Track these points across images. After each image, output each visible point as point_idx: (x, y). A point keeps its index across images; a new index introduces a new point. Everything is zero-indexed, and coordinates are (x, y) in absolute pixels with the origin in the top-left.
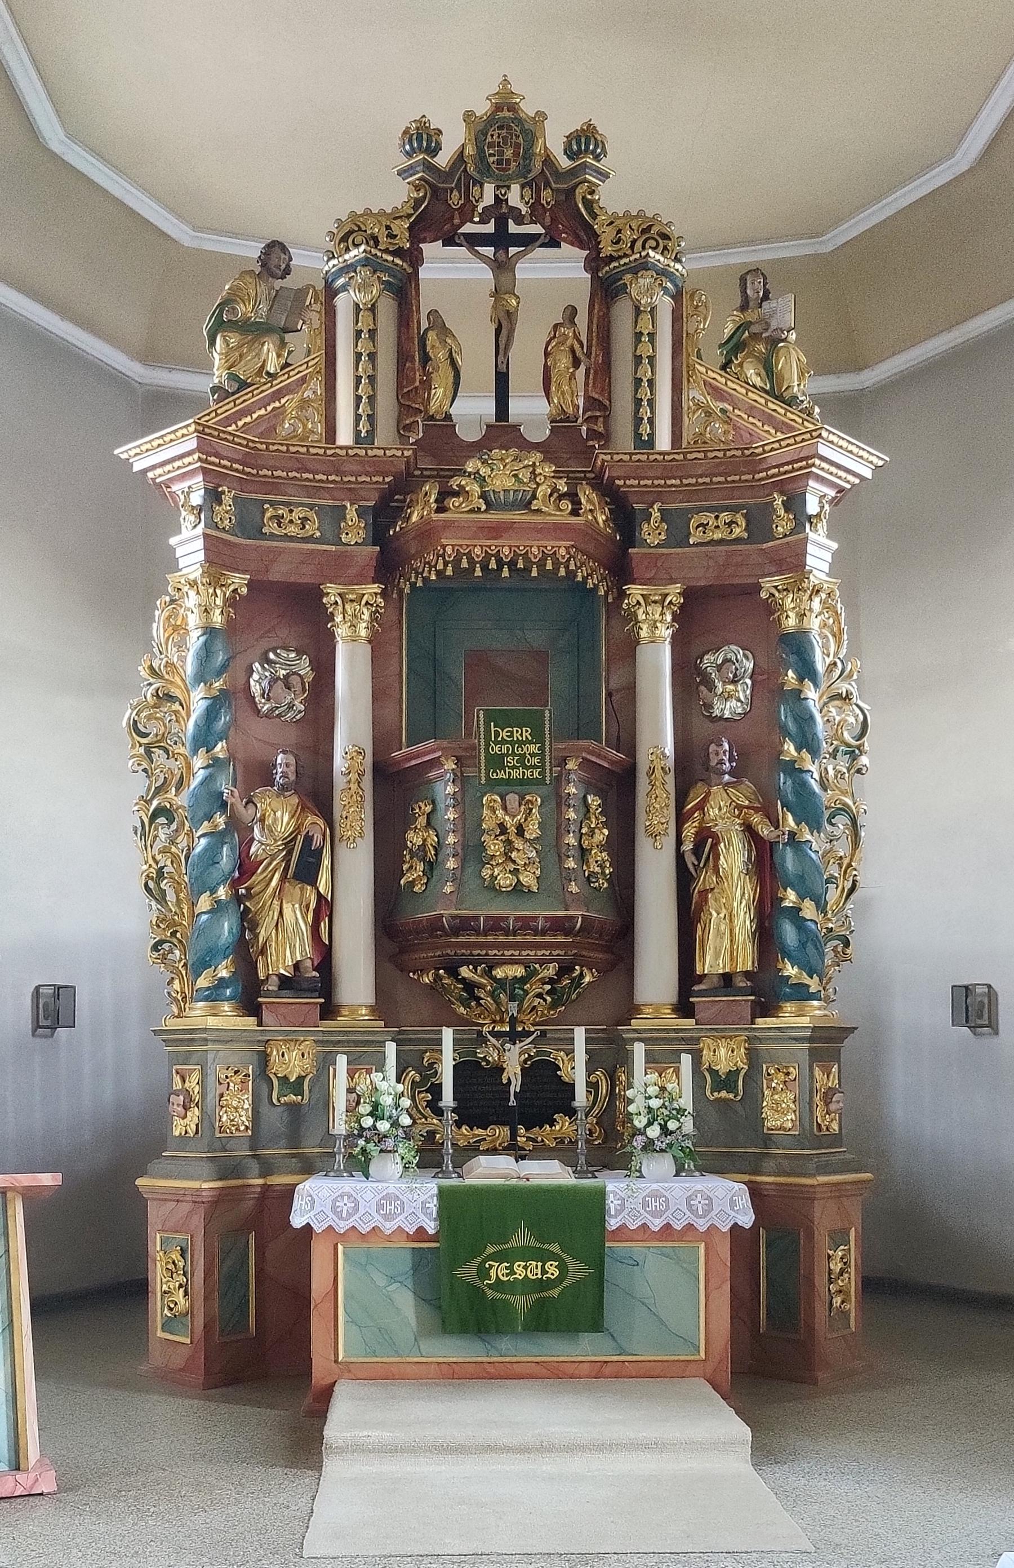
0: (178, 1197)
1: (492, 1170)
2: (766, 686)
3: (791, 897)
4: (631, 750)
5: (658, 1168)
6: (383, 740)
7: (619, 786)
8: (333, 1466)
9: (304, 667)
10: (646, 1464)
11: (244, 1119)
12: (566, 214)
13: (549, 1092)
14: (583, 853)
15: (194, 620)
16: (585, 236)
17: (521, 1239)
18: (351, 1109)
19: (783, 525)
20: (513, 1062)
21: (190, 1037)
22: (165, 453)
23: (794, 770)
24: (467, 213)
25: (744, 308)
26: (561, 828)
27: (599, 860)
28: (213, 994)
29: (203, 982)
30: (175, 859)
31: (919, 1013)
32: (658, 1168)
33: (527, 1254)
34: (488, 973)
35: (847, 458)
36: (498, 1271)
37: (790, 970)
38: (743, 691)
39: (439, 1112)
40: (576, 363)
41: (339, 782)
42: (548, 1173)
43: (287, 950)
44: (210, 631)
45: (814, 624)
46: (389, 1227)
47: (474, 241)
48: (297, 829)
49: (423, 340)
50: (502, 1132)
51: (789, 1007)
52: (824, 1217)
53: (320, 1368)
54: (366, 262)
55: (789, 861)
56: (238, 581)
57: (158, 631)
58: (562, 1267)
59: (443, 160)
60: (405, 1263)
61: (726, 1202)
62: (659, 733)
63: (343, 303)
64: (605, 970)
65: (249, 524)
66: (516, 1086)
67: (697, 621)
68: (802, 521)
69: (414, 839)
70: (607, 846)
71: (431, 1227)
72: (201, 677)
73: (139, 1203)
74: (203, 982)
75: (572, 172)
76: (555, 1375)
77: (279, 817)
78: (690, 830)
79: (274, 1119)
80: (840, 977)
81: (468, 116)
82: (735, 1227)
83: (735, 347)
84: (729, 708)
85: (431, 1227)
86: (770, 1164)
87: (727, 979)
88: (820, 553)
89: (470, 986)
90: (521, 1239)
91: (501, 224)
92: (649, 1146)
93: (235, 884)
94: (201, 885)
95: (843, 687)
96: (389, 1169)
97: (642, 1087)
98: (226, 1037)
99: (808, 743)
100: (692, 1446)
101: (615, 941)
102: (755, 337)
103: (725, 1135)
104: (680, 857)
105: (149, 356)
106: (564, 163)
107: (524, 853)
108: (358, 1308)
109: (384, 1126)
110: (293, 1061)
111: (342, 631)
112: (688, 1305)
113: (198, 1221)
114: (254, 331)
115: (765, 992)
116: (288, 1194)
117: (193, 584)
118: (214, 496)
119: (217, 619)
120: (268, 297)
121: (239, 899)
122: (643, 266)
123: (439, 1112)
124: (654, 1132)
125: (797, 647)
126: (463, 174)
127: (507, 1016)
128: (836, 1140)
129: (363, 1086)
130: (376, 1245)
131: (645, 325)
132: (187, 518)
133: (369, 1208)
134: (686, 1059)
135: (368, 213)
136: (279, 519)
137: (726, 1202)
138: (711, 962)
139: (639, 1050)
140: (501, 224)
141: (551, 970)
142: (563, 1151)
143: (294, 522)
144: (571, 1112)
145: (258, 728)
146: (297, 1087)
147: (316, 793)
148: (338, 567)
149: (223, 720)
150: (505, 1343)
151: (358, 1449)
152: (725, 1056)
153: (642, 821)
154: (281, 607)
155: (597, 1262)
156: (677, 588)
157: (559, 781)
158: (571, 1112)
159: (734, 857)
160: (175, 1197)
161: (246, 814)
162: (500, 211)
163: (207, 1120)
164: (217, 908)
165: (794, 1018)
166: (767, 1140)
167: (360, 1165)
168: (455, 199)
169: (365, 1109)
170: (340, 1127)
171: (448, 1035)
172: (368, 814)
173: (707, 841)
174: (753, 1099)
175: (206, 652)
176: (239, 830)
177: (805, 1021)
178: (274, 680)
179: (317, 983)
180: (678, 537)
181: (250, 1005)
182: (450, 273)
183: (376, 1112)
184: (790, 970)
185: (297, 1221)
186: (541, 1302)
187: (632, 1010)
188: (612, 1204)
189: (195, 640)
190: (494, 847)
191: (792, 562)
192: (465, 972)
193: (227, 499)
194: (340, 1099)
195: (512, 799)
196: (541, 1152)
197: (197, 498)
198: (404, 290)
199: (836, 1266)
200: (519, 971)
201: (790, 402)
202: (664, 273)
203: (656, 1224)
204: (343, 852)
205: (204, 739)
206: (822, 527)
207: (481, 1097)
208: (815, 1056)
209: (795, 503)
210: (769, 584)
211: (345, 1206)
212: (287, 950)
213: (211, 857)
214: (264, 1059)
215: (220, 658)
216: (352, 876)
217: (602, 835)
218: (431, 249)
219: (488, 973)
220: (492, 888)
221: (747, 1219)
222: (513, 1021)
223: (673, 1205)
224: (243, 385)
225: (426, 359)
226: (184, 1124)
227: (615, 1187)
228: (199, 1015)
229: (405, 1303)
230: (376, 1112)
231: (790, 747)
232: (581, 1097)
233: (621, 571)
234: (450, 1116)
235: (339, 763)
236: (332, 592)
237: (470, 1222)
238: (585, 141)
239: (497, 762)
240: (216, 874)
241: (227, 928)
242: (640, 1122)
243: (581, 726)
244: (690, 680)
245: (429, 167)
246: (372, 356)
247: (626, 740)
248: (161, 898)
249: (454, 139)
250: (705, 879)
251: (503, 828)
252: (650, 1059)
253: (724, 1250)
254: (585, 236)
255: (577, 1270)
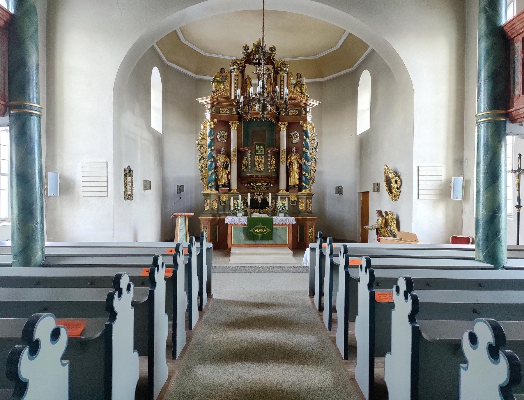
0: (206, 220)
1: (256, 215)
2: (301, 138)
3: (304, 173)
4: (279, 149)
5: (281, 215)
6: (239, 146)
7: (277, 154)
8: (232, 256)
9: (226, 134)
10: (277, 256)
11: (216, 207)
12: (270, 60)
13: (264, 204)
14: (271, 165)
15: (208, 127)
16: (272, 64)
17: (260, 225)
18: (234, 206)
19: (304, 113)
20: (259, 199)
21: (208, 194)
22: (204, 101)
23: (305, 152)
24: (253, 59)
25: (297, 79)
26: (267, 161)
27: (274, 166)
28: (211, 187)
29: (210, 185)
30: (205, 165)
31: (331, 191)
32: (281, 215)
33: (261, 228)
34: (256, 184)
35: (313, 103)
36: (257, 230)
37: (304, 184)
38: (297, 139)
39: (247, 207)
40: (271, 84)
41: (232, 153)
42: (265, 216)
43: (223, 180)
44: (211, 129)
45: (308, 129)
46: (240, 223)
47: (254, 64)
48: (225, 161)
49: (246, 80)
50: (258, 210)
51: (304, 190)
52: (308, 223)
53: (229, 246)
54: (237, 68)
55: (304, 167)
56: (216, 120)
57: (202, 127)
58: (266, 230)
59: (249, 51)
60: (242, 229)
61: (292, 220)
62: (284, 146)
63: (233, 74)
64: (275, 184)
65: (218, 111)
66: (260, 202)
67: (290, 127)
68: (307, 112)
69: (244, 162)
70: (275, 164)
71: (246, 224)
72: (210, 136)
73: (199, 221)
74: (210, 185)
75: (271, 54)
76: (265, 246)
77: (222, 159)
78: (288, 162)
79: (221, 207)
80: (313, 186)
81: (254, 44)
82: (293, 224)
83: (296, 85)
84: (295, 141)
85: (246, 224)
86: (300, 215)
87: (294, 186)
88: (309, 118)
89: (253, 186)
90: (260, 225)
91: (259, 61)
92: (280, 212)
93: (215, 169)
94: (210, 170)
95: (314, 138)
96: (240, 215)
97: (280, 202)
98: (213, 194)
99: (307, 148)
100: (283, 254)
101: (276, 180)
102: (299, 84)
103: (293, 210)
104: (287, 166)
105: (196, 73)
106: (270, 52)
107: (261, 165)
108: (235, 236)
109: (239, 208)
110: (224, 198)
111: (232, 128)
112: (286, 236)
113: (209, 223)
114: (219, 82)
115: (300, 188)
116: (224, 219)
117: (209, 121)
118: (212, 107)
119: (212, 127)
120: (223, 77)
121: (215, 172)
122: (282, 70)
123: (247, 207)
124: (281, 209)
125: (306, 132)
126: (252, 53)
127: (258, 190)
128: (311, 211)
129: (236, 202)
130: (238, 226)
131: (282, 79)
132: (208, 111)
133: (236, 221)
134: (287, 198)
135: (237, 59)
136: (222, 110)
137: (292, 220)
138: (292, 183)
139: (279, 197)
140: (259, 61)
141: (266, 184)
142: (267, 213)
143: (225, 111)
144: (269, 207)
145: (218, 144)
146: (225, 202)
147: (228, 154)
148: (232, 118)
149: (213, 142)
150: (257, 242)
151: (236, 254)
152: (293, 198)
153: (281, 160)
154: (222, 124)
155: (272, 229)
156: (287, 122)
157: (267, 154)
158: (269, 207)
159: (295, 166)
160: (205, 219)
161: (217, 158)
162: (259, 59)
163: (210, 207)
164: (212, 174)
165: (304, 192)
166: (300, 211)
167: (235, 214)
168: (251, 57)
169: (236, 205)
170: (232, 209)
171: (249, 194)
172: (236, 158)
173: (291, 163)
174: (298, 205)
175: (211, 132)
176: (216, 161)
177: (306, 193)
178: (221, 136)
179: (228, 185)
180: (287, 114)
181: (217, 189)
182: (250, 69)
183: (238, 206)
184: (304, 184)
185: (226, 222)
186: (263, 235)
187: (279, 190)
188: (274, 220)
189: (209, 130)
190: (257, 164)
191: (305, 119)
192: (252, 184)
193: (214, 108)
194: (232, 204)
195: (260, 156)
196: (264, 213)
197: (209, 107)
198: (243, 72)
199: (310, 231)
200: (260, 184)
201: (304, 95)
202: (285, 71)
203: (281, 223)
204: (232, 164)
205: (210, 146)
206: (310, 113)
207: (254, 205)
208: (307, 198)
209: (305, 109)
210: (301, 122)
211: (233, 220)
212: (223, 180)
213: (211, 165)
214: (219, 198)
215: (213, 133)
216: (234, 168)
217: (274, 162)
218: (248, 65)
219: (256, 184)
220: (256, 171)
221: (295, 223)
222: (260, 192)
223: (283, 221)
224: (217, 91)
225: (246, 83)
226: (207, 208)
227: (274, 218)
228: (209, 191)
229: (242, 235)
230: (238, 206)
231: (304, 149)
232: (270, 204)
233: (278, 119)
234: (249, 207)
235: (232, 150)
236: (231, 122)
237: (252, 223)
238: (273, 49)
239: (257, 151)
240: (212, 168)
241: (214, 177)
242: (278, 208)
243: (271, 145)
244: (289, 137)
245: (247, 52)
246: (238, 83)
247: (278, 147)
248: (202, 171)
249: (251, 48)
250: (291, 170)
251: (258, 161)
252: (281, 198)
253: (291, 228)
254: (272, 64)
255: (269, 230)
